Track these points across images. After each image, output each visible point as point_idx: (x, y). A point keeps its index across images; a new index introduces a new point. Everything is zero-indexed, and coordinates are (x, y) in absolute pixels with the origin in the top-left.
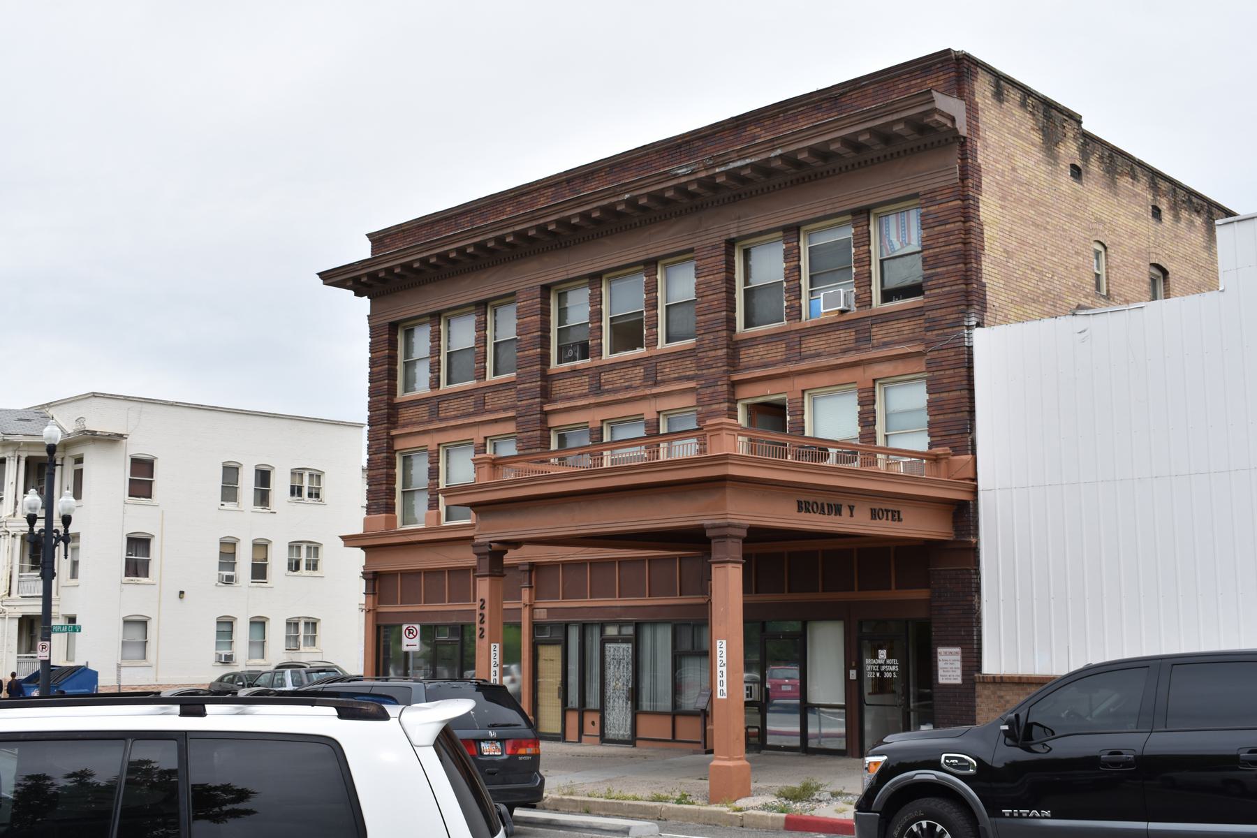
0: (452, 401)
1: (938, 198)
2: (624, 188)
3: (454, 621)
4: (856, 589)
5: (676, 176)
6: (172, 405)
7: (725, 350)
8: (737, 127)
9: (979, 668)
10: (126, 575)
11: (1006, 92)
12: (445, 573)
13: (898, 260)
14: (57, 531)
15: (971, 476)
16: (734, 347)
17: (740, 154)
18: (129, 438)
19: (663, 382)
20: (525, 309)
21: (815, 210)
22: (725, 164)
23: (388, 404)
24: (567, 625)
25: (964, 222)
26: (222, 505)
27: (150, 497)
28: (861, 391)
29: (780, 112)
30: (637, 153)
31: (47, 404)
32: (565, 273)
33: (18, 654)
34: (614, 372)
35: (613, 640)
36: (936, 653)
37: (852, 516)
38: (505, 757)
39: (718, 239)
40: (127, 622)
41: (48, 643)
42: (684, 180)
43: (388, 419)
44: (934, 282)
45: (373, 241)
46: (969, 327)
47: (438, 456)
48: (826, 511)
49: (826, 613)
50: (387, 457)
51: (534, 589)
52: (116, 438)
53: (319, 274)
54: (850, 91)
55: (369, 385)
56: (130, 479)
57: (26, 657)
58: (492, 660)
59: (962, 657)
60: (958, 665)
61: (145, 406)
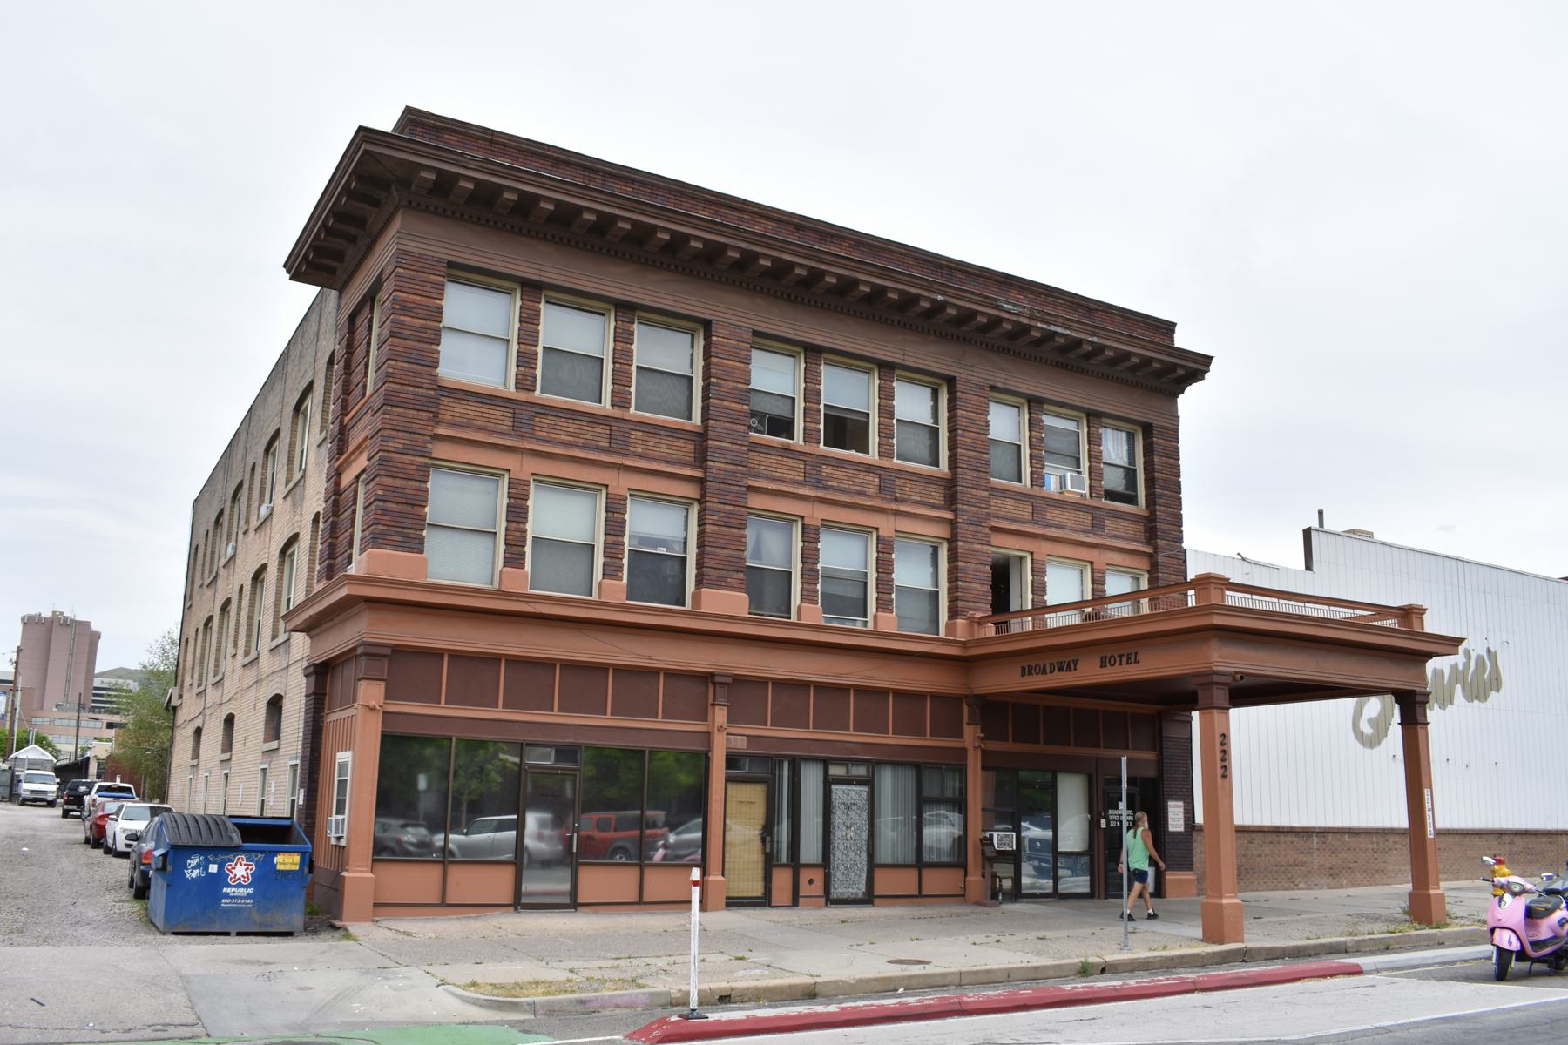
0: (563, 420)
2: (942, 288)
3: (571, 741)
4: (1042, 742)
12: (888, 695)
13: (1112, 467)
17: (1066, 322)
19: (903, 501)
20: (727, 349)
21: (1074, 398)
22: (1048, 323)
29: (1043, 294)
30: (655, 180)
34: (840, 469)
36: (1167, 805)
39: (983, 381)
42: (1004, 315)
44: (1163, 501)
49: (1072, 766)
59: (1185, 809)
60: (1182, 816)
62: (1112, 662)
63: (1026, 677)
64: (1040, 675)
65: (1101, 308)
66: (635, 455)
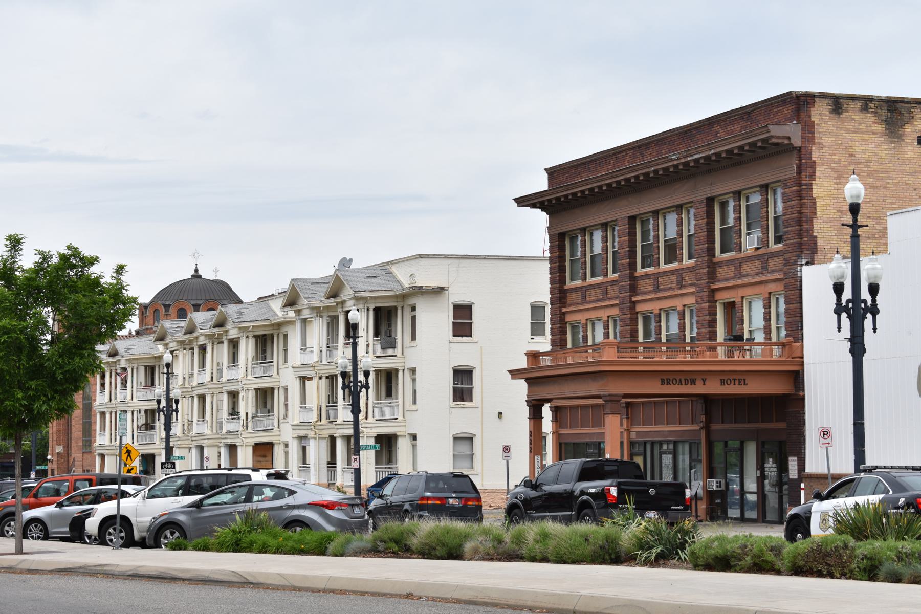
1: (789, 184)
4: (774, 421)
5: (672, 160)
6: (485, 258)
7: (707, 269)
8: (710, 124)
9: (804, 470)
10: (454, 401)
11: (845, 106)
14: (361, 382)
15: (800, 355)
16: (713, 267)
18: (450, 289)
23: (559, 290)
24: (645, 443)
25: (800, 200)
26: (532, 339)
27: (471, 336)
28: (764, 299)
31: (390, 262)
32: (638, 210)
33: (376, 464)
35: (665, 453)
37: (704, 384)
38: (461, 505)
40: (456, 439)
41: (358, 457)
43: (560, 300)
45: (549, 174)
46: (802, 265)
47: (587, 327)
48: (683, 383)
50: (560, 327)
51: (558, 423)
52: (439, 290)
53: (514, 199)
54: (755, 110)
55: (550, 276)
56: (453, 322)
57: (386, 468)
58: (536, 465)
61: (462, 261)
62: (729, 383)
63: (665, 385)
64: (677, 385)
65: (752, 109)
66: (664, 290)
